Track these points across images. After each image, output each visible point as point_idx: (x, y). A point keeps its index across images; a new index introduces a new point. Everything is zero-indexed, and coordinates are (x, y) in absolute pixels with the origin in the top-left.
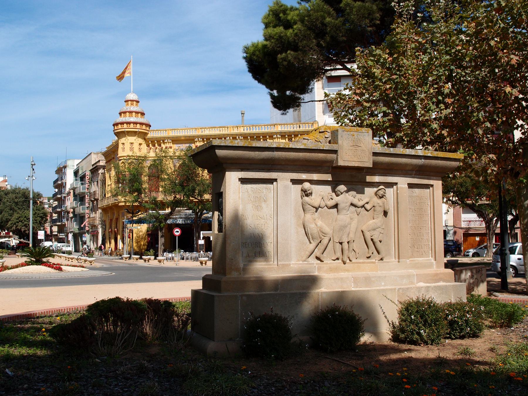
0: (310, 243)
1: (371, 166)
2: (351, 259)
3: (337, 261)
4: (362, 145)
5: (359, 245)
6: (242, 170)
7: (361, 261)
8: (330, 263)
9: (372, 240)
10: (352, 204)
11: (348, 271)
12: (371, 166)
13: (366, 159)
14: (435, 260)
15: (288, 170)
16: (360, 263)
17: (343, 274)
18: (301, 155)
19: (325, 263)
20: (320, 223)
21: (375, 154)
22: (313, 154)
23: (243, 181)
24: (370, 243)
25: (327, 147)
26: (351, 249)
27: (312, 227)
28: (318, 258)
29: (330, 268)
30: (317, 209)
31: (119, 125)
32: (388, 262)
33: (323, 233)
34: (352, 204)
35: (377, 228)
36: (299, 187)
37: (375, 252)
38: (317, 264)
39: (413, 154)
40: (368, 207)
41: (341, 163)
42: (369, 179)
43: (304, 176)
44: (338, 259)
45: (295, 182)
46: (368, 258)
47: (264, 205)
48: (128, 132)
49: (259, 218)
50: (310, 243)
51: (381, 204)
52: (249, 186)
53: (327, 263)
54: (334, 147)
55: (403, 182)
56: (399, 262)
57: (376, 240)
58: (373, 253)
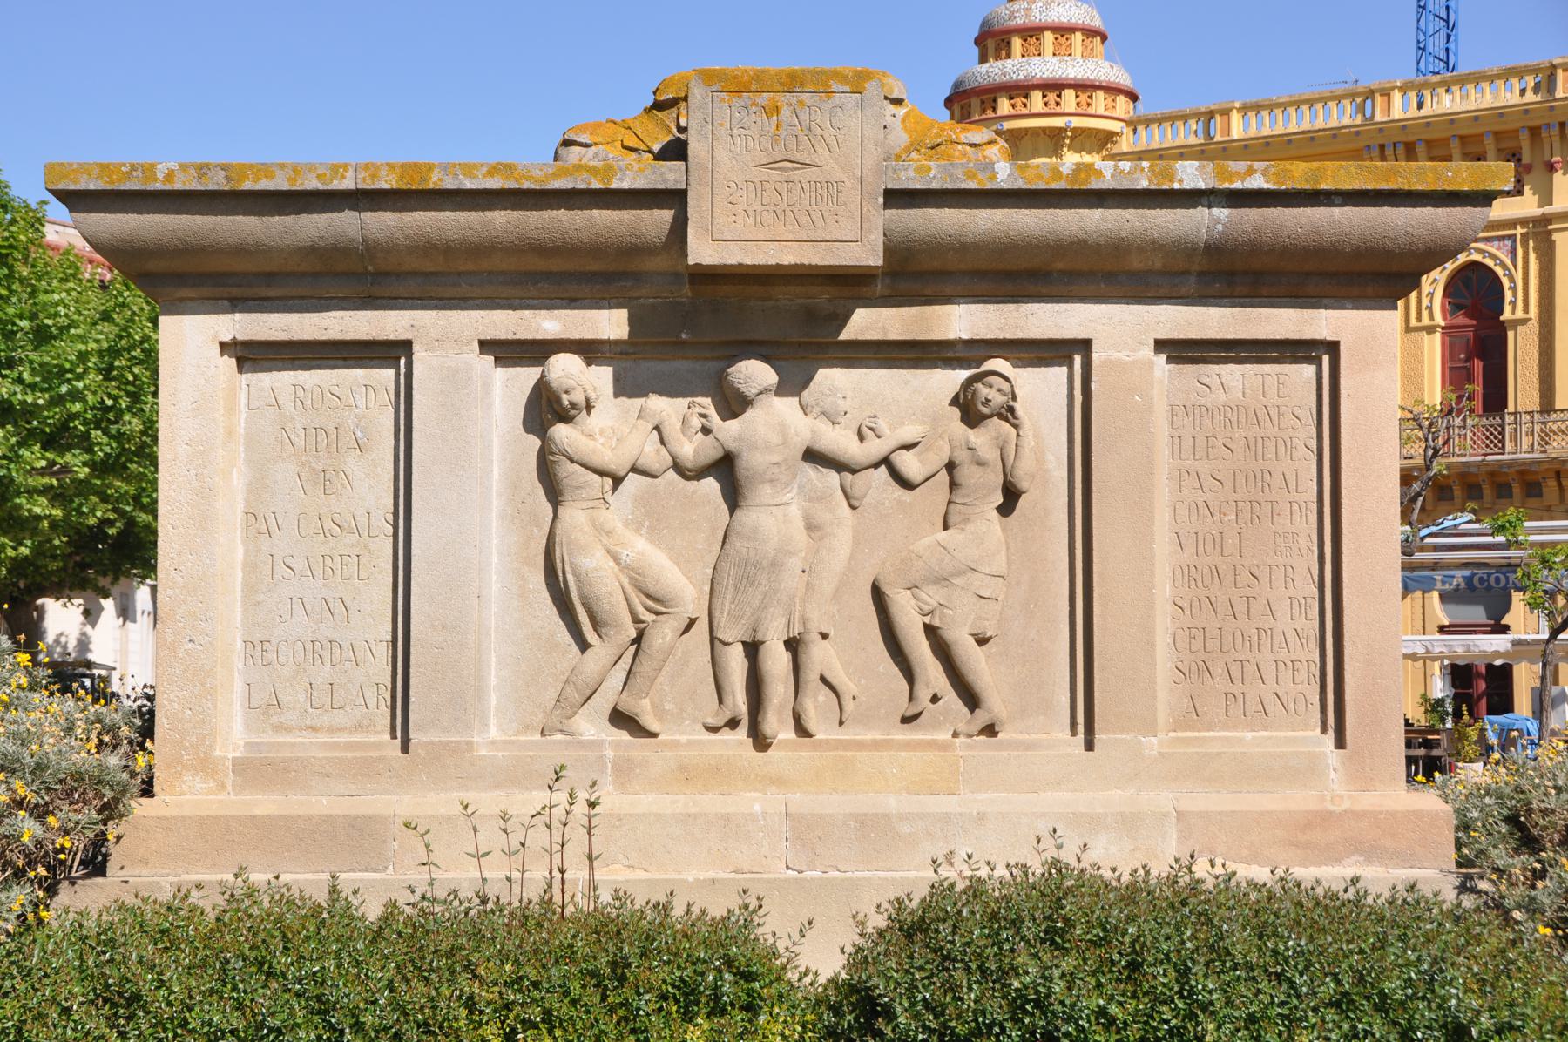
0: (584, 645)
1: (876, 260)
2: (811, 723)
3: (727, 735)
4: (822, 156)
5: (849, 654)
6: (237, 304)
7: (870, 736)
8: (690, 743)
9: (931, 631)
10: (813, 456)
11: (779, 782)
12: (876, 260)
13: (848, 229)
14: (1340, 743)
15: (465, 299)
16: (860, 745)
17: (753, 802)
18: (500, 220)
19: (665, 744)
20: (639, 547)
21: (896, 198)
22: (289, 220)
23: (251, 355)
24: (920, 650)
25: (636, 174)
26: (811, 676)
27: (597, 571)
28: (621, 719)
29: (682, 768)
30: (617, 481)
31: (1036, 96)
32: (1030, 746)
33: (649, 596)
34: (813, 456)
35: (960, 573)
36: (527, 377)
37: (950, 697)
38: (617, 745)
39: (1143, 184)
40: (910, 464)
41: (702, 251)
42: (865, 323)
43: (548, 324)
44: (733, 724)
45: (506, 352)
46: (906, 720)
47: (353, 464)
48: (1079, 133)
49: (328, 525)
50: (584, 645)
51: (990, 454)
52: (283, 380)
53: (675, 745)
54: (670, 175)
55: (1121, 330)
56: (1089, 746)
57: (960, 638)
58: (935, 699)
